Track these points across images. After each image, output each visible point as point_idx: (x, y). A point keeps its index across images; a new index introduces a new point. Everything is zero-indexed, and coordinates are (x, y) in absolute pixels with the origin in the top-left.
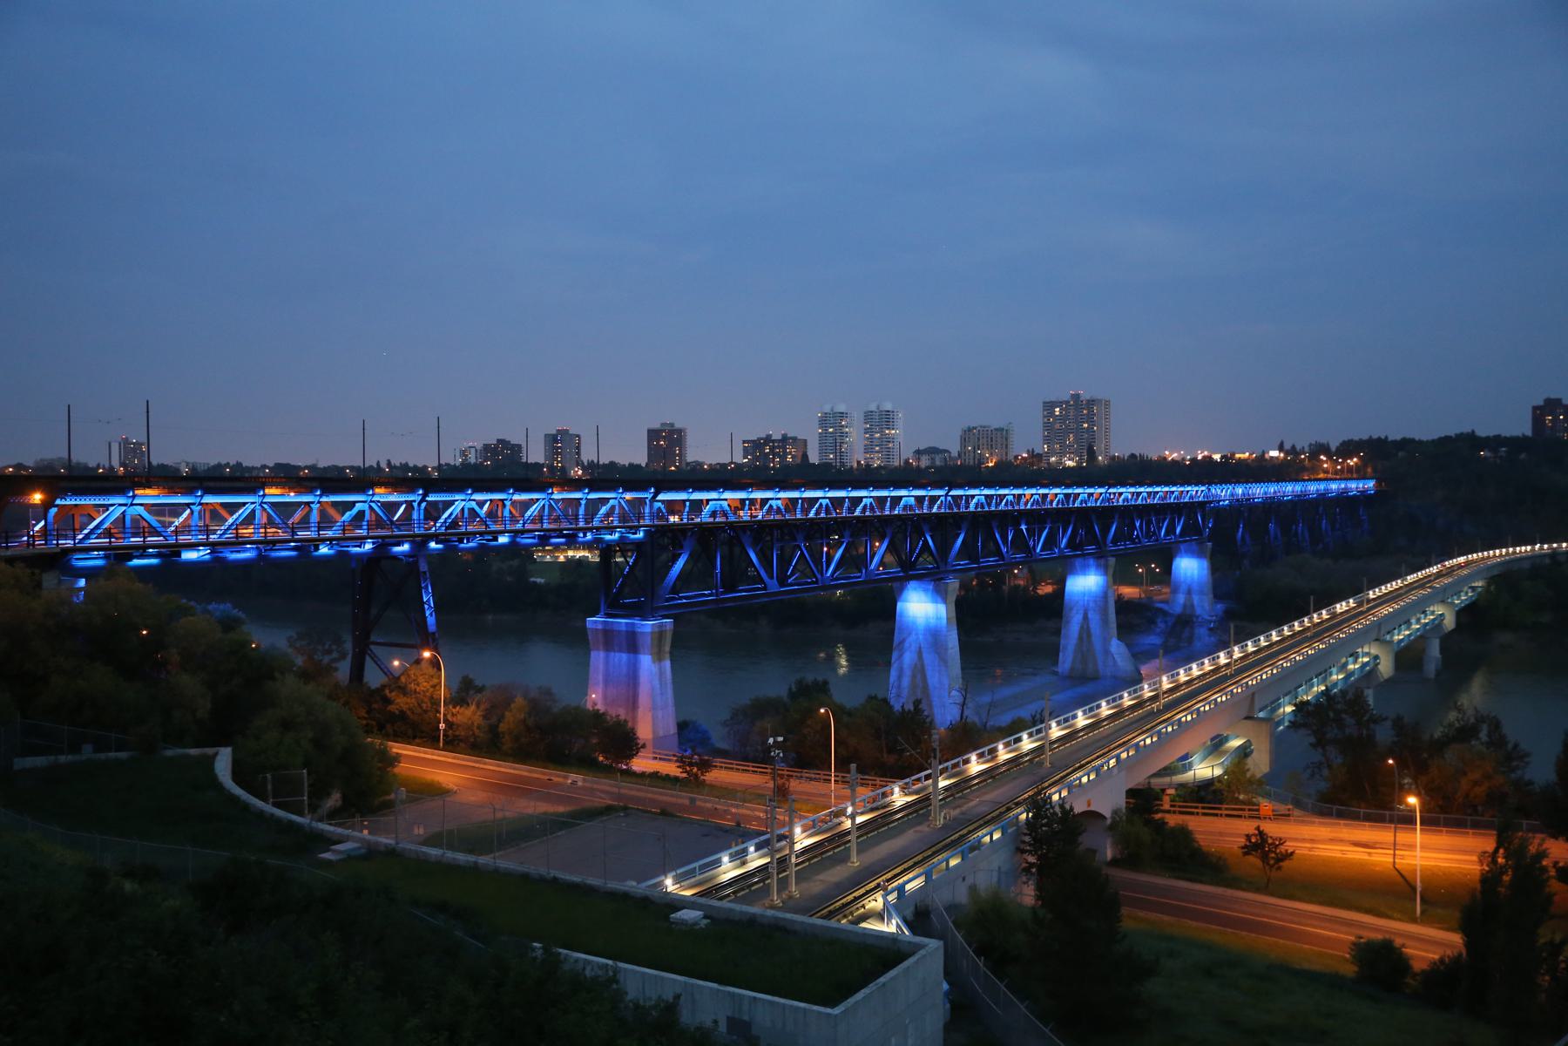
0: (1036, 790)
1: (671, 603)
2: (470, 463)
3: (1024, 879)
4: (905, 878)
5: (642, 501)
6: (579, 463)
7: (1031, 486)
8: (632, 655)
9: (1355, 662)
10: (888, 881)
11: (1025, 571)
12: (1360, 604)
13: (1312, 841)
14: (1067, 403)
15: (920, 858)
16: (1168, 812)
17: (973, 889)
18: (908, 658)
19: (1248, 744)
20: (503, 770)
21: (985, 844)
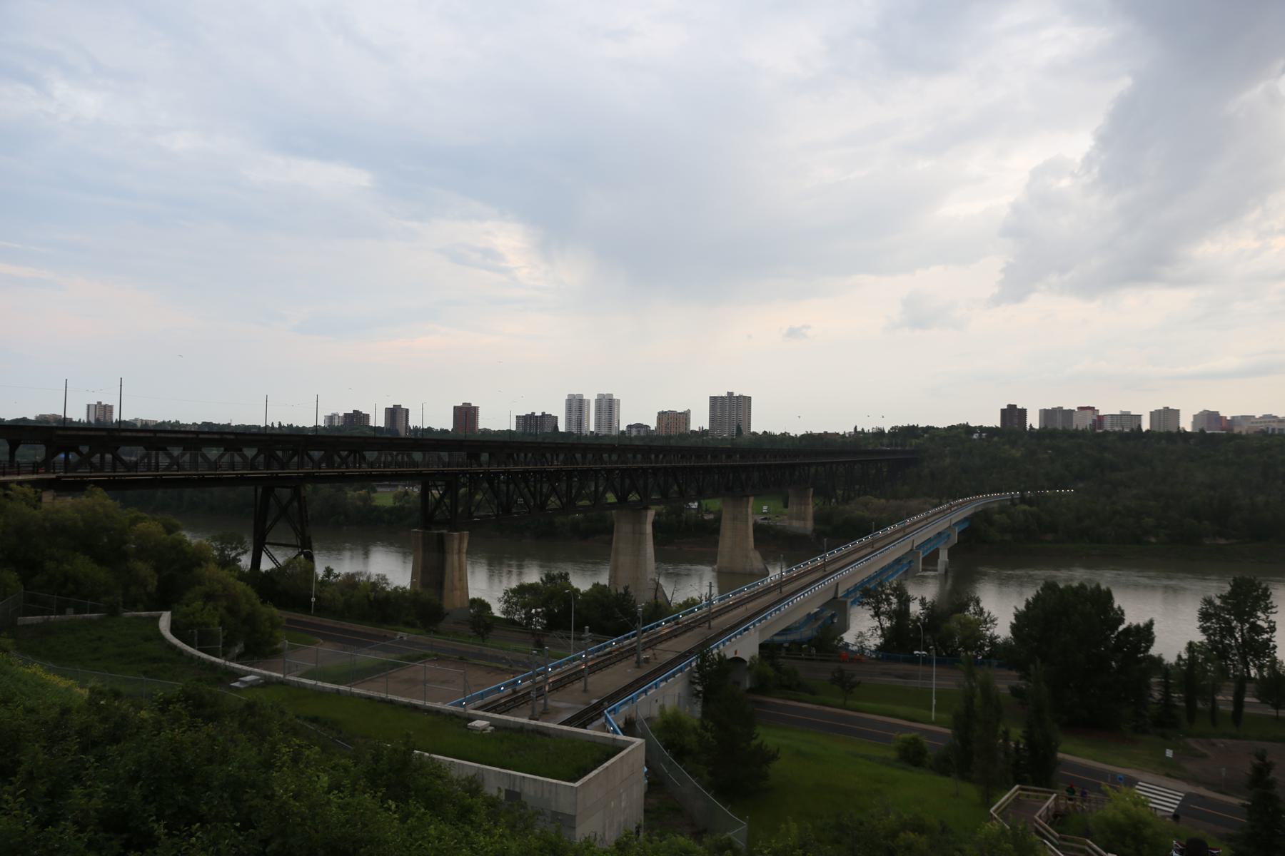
17: (662, 707)
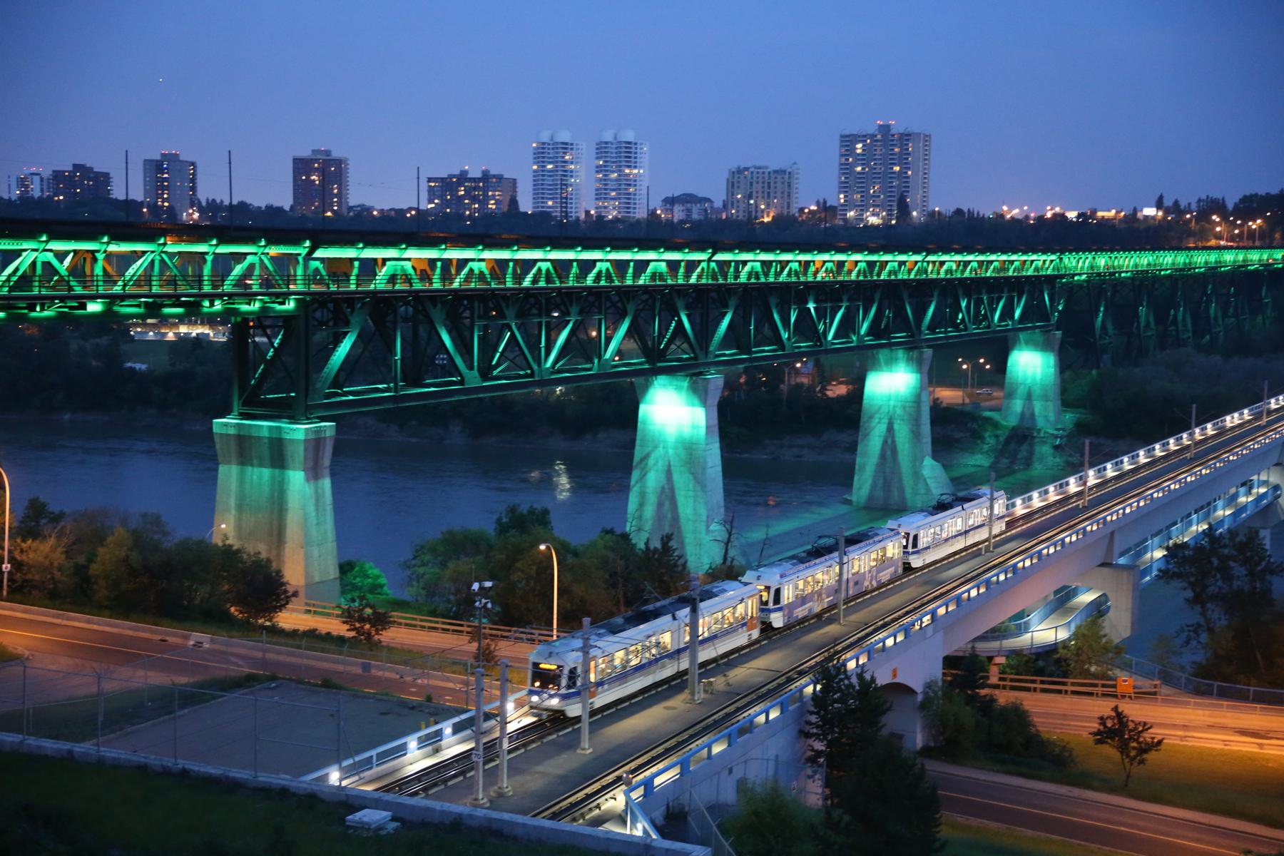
0: (826, 654)
1: (333, 400)
2: (33, 197)
3: (809, 772)
4: (654, 770)
5: (292, 258)
6: (194, 202)
7: (823, 249)
8: (277, 471)
9: (1249, 493)
10: (632, 772)
11: (811, 365)
12: (1258, 416)
13: (1185, 727)
14: (872, 136)
15: (672, 742)
16: (996, 687)
17: (741, 785)
18: (653, 479)
19: (1103, 599)
20: (95, 627)
21: (758, 726)
